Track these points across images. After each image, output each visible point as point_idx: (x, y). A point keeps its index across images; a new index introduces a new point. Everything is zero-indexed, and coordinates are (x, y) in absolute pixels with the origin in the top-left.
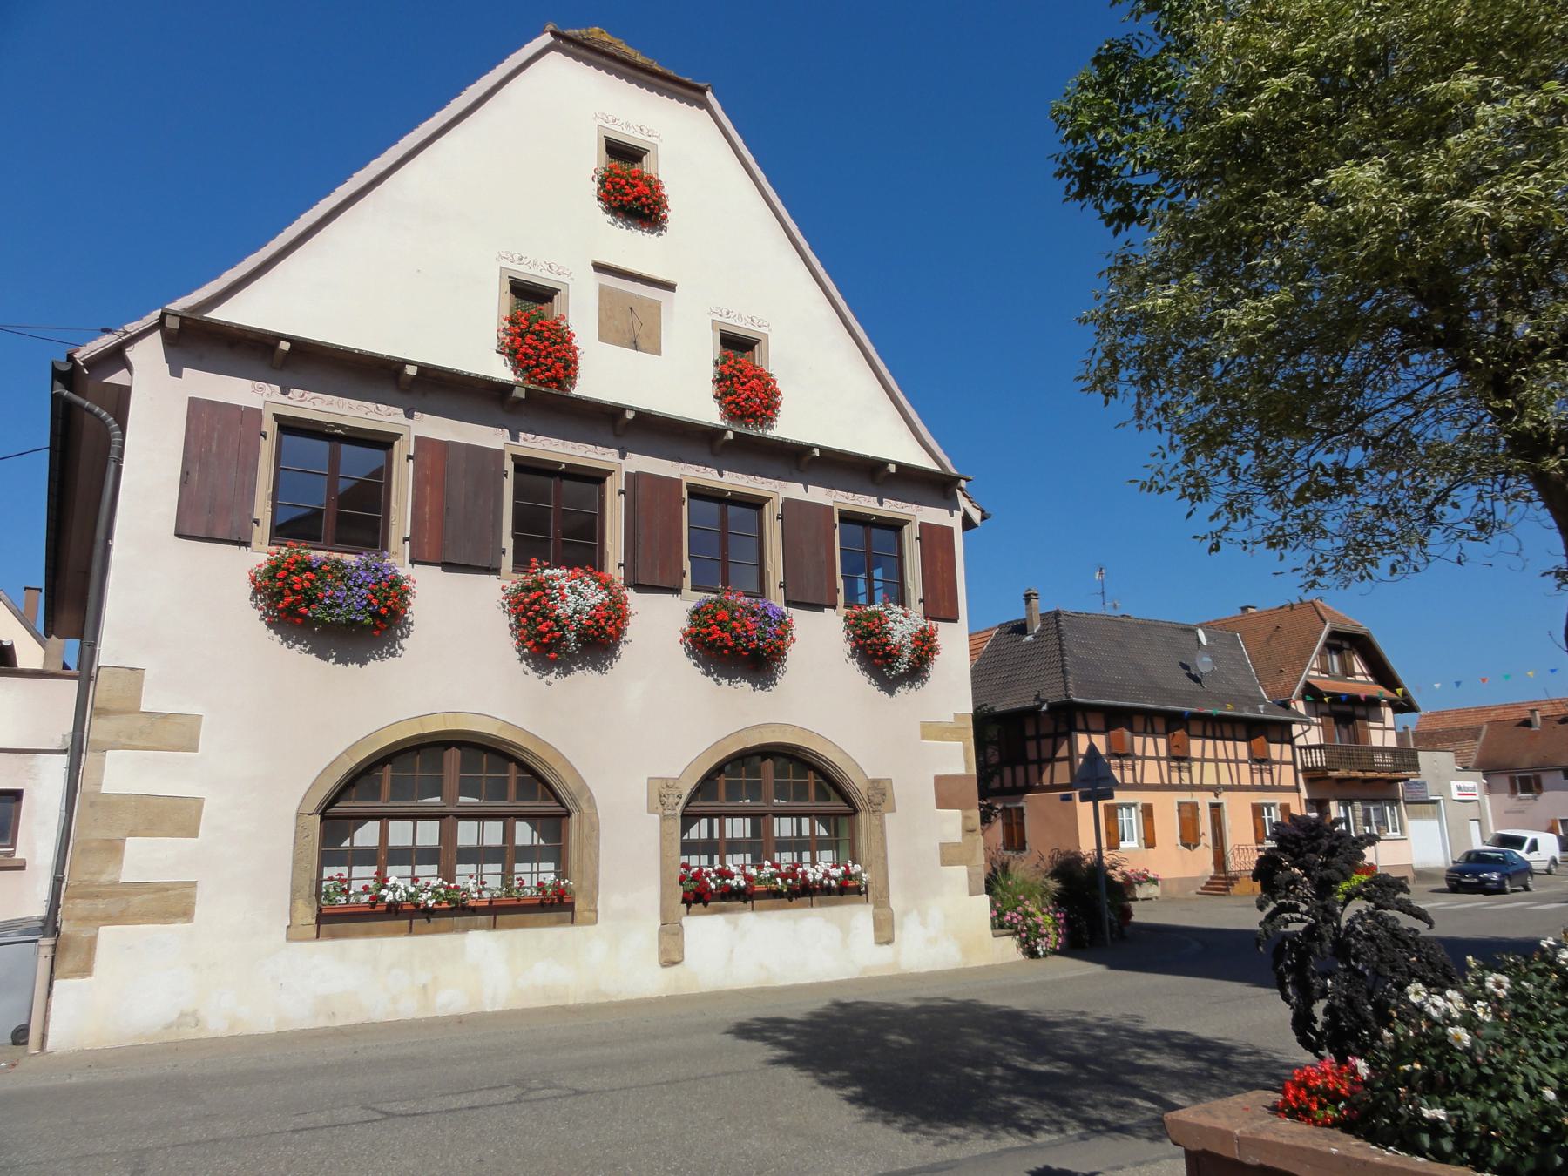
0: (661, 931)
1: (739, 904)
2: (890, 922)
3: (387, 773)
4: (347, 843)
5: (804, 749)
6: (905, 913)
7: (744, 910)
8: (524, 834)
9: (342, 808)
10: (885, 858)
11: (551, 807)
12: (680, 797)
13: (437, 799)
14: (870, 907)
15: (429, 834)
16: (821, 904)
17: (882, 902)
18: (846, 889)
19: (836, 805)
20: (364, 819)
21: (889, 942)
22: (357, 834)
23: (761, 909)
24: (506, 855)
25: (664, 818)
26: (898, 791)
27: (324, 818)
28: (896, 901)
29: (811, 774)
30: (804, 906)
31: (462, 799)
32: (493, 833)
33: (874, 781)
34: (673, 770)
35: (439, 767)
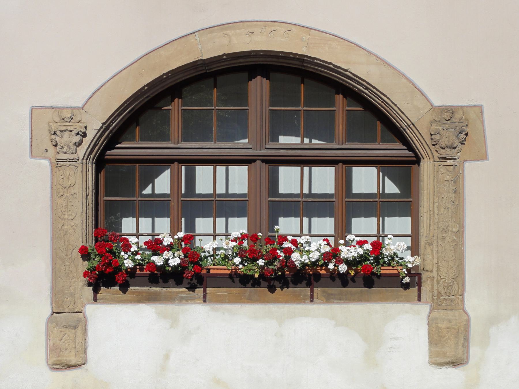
0: (49, 320)
1: (182, 290)
2: (463, 333)
3: (176, 108)
4: (148, 190)
5: (312, 60)
6: (494, 320)
7: (188, 300)
8: (365, 180)
9: (126, 148)
10: (460, 233)
11: (394, 150)
12: (85, 135)
13: (246, 141)
14: (424, 309)
15: (238, 180)
16: (329, 299)
17: (450, 298)
18: (369, 276)
19: (394, 150)
20: (165, 162)
21: (455, 363)
22: (157, 181)
23: (220, 300)
24: (346, 206)
25: (58, 164)
26: (494, 129)
27: (101, 163)
28: (476, 301)
29: (340, 98)
30: (297, 299)
31: (283, 139)
32: (323, 180)
33: (443, 109)
34: (72, 96)
35: (242, 98)
